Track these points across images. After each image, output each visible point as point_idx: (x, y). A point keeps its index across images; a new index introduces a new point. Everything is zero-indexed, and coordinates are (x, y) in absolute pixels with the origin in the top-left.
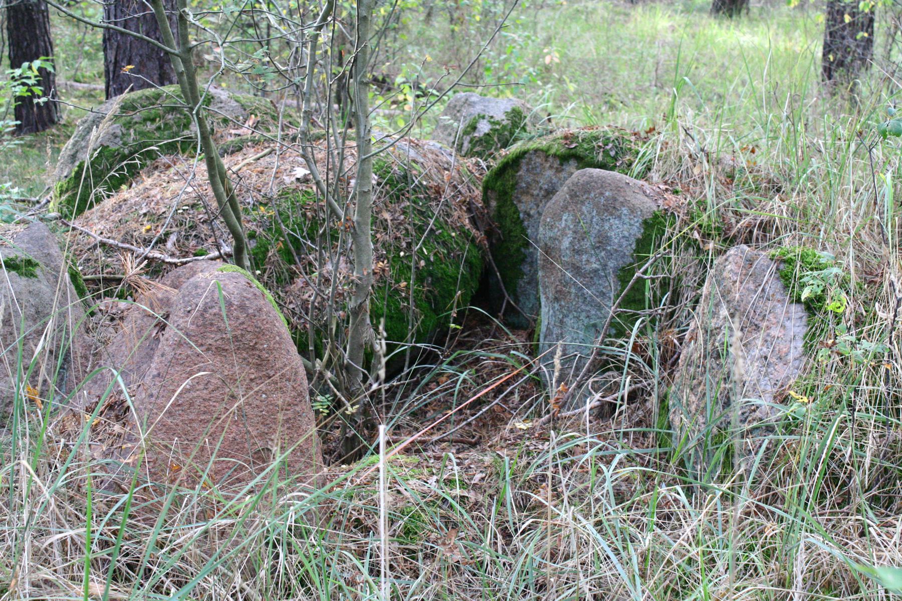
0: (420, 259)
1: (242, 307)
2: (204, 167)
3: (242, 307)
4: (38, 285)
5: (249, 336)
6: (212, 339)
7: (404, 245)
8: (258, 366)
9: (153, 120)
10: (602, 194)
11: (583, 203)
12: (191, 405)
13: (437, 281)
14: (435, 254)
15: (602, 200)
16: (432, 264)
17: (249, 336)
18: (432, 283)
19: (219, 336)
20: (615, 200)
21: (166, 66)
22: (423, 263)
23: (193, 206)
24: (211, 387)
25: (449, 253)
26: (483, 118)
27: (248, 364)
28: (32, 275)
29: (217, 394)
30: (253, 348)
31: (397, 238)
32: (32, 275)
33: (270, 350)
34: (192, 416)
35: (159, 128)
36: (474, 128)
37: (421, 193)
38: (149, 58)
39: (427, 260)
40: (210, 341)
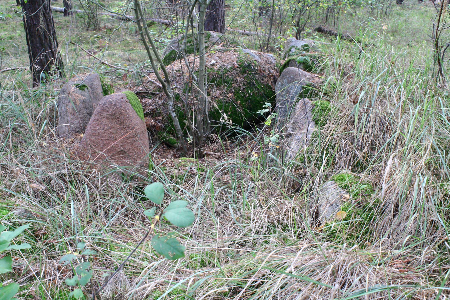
0: (247, 94)
1: (115, 105)
2: (439, 44)
3: (115, 105)
4: (85, 93)
5: (117, 114)
6: (105, 114)
7: (242, 89)
8: (120, 124)
9: (190, 42)
10: (290, 76)
11: (284, 79)
12: (99, 134)
13: (252, 102)
14: (253, 93)
15: (290, 79)
16: (251, 96)
17: (117, 114)
18: (250, 102)
19: (107, 113)
20: (294, 79)
21: (216, 25)
22: (247, 95)
23: (178, 71)
24: (105, 129)
25: (259, 93)
26: (294, 47)
27: (117, 123)
28: (83, 90)
29: (107, 131)
30: (118, 118)
31: (240, 86)
32: (83, 90)
33: (124, 119)
34: (99, 138)
35: (191, 45)
36: (290, 50)
37: (253, 71)
38: (211, 21)
39: (249, 94)
40: (105, 115)
